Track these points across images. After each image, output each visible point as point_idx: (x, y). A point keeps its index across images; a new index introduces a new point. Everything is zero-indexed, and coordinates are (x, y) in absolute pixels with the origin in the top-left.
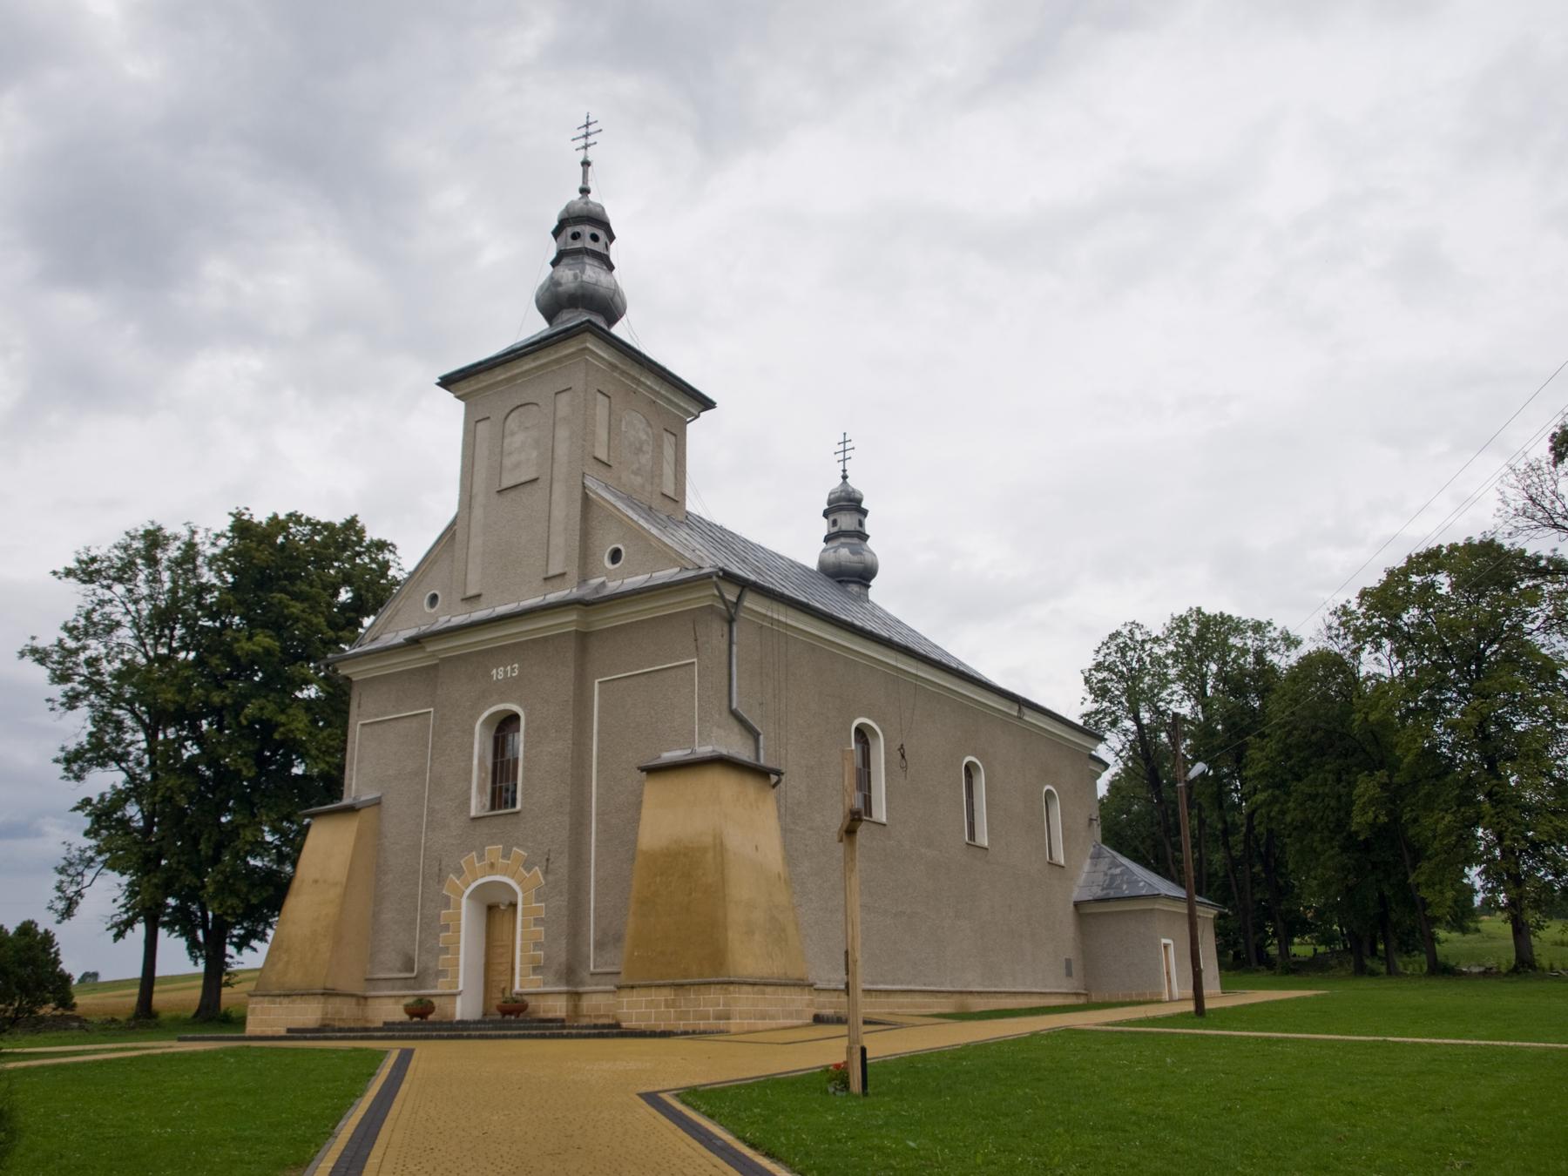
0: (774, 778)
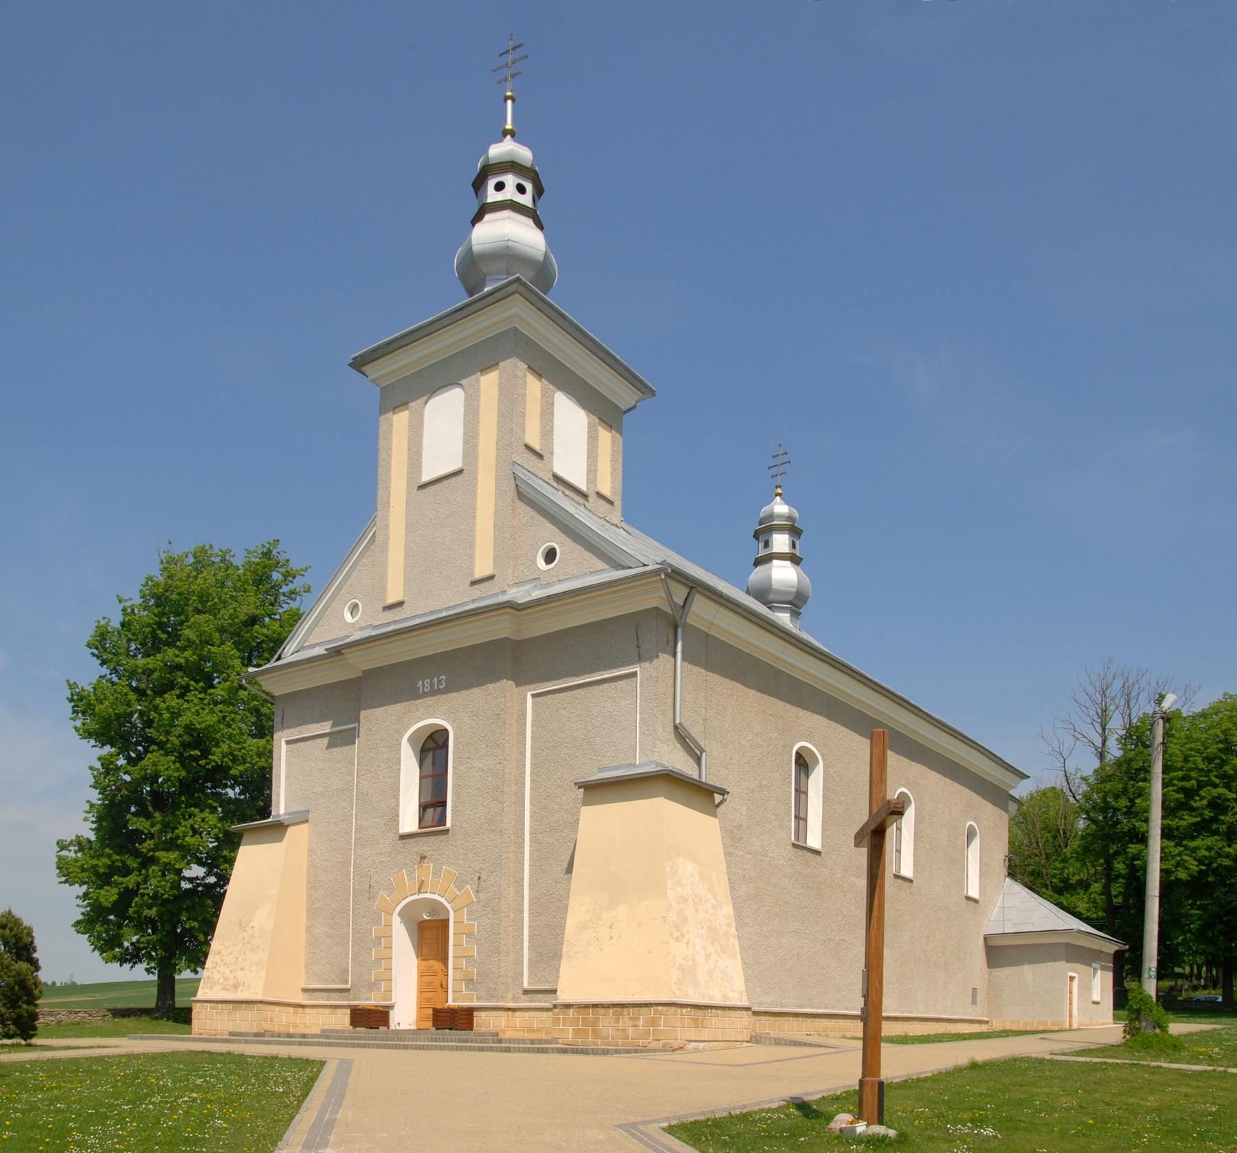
0: (718, 798)
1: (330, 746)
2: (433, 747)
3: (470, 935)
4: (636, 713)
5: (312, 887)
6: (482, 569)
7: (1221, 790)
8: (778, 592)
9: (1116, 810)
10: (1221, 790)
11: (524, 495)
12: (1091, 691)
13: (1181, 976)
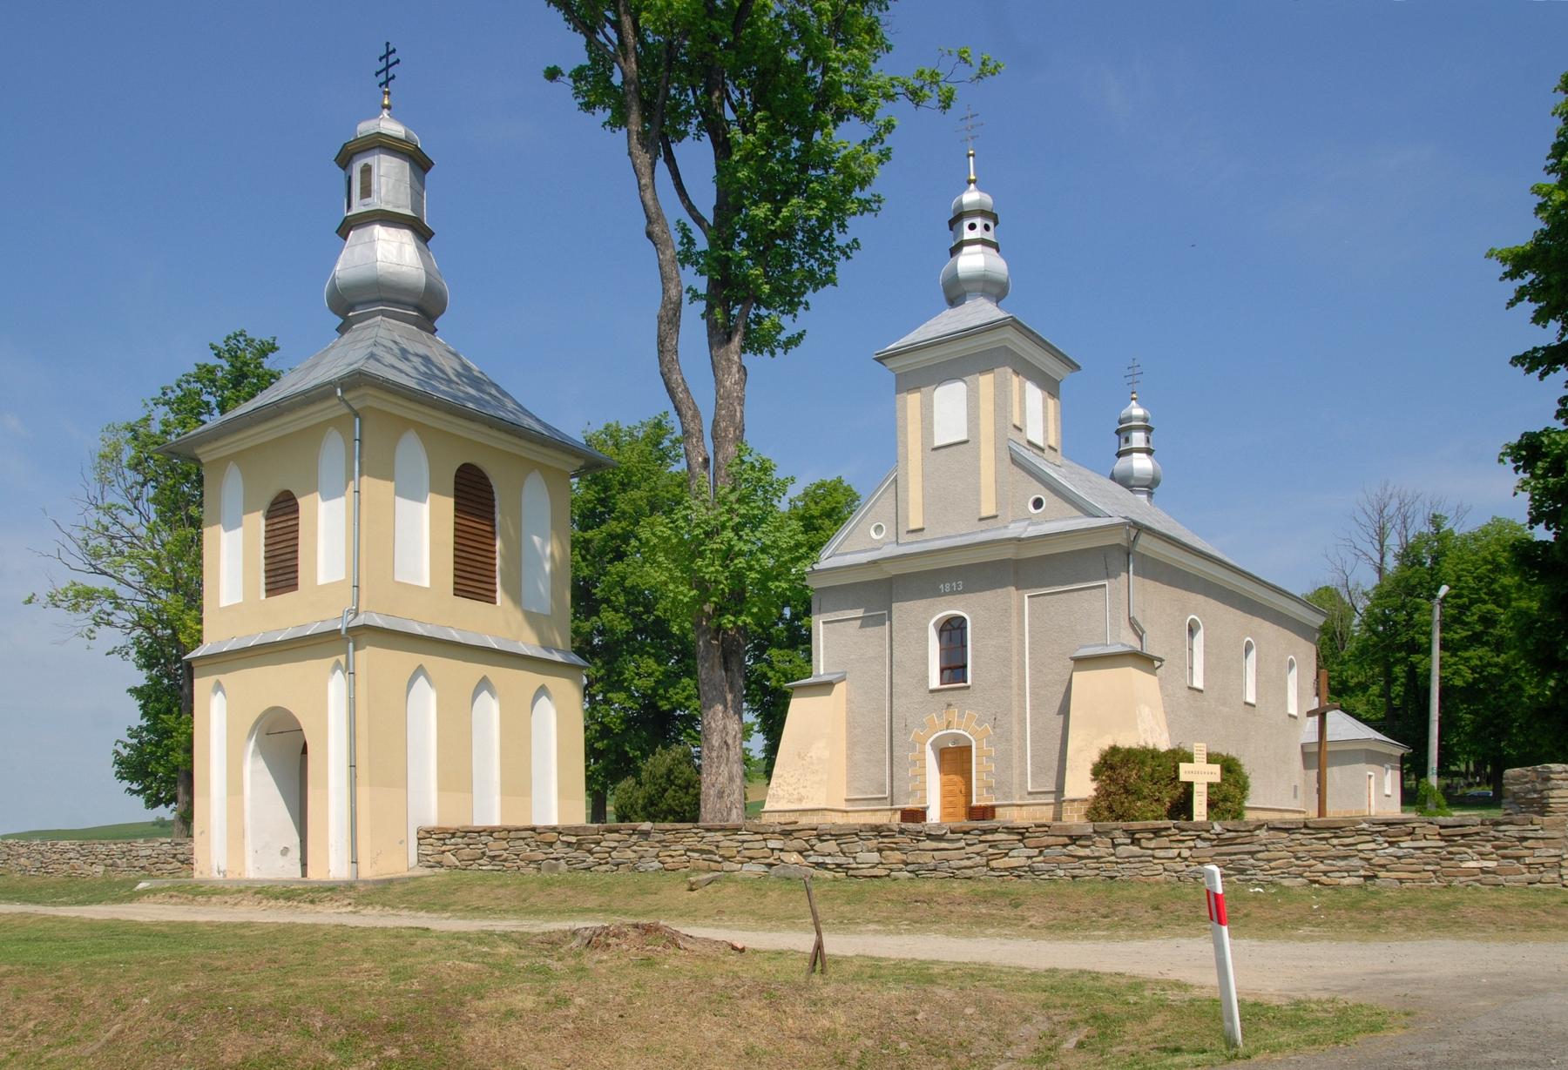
0: (1157, 664)
1: (862, 626)
2: (953, 631)
3: (989, 757)
4: (1105, 609)
5: (851, 726)
6: (988, 509)
7: (1490, 606)
8: (1138, 479)
9: (1395, 623)
10: (1490, 606)
11: (1016, 461)
12: (1369, 509)
13: (1457, 774)
